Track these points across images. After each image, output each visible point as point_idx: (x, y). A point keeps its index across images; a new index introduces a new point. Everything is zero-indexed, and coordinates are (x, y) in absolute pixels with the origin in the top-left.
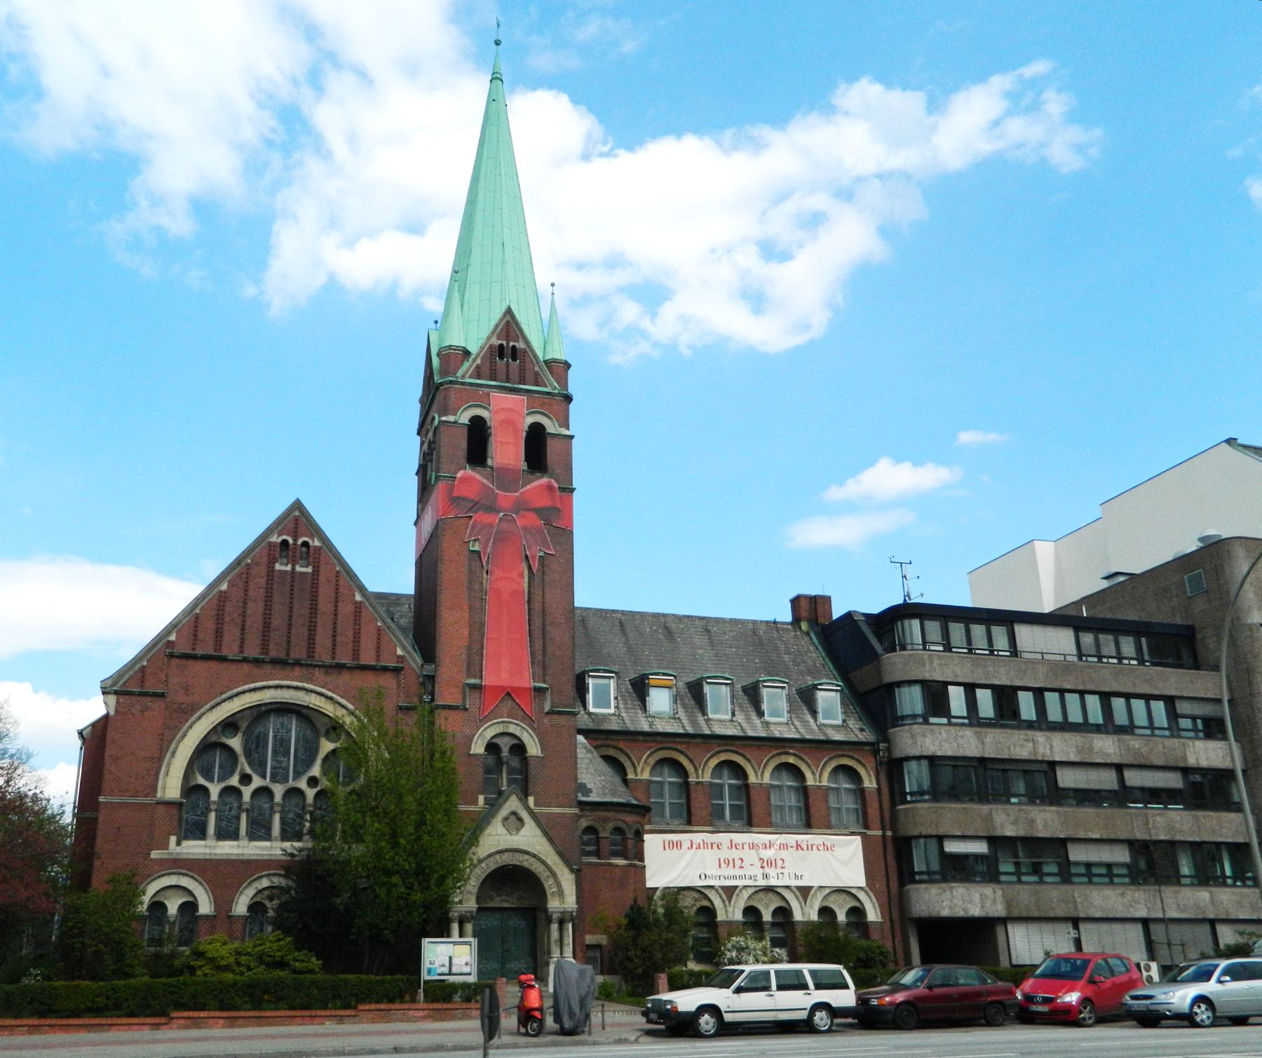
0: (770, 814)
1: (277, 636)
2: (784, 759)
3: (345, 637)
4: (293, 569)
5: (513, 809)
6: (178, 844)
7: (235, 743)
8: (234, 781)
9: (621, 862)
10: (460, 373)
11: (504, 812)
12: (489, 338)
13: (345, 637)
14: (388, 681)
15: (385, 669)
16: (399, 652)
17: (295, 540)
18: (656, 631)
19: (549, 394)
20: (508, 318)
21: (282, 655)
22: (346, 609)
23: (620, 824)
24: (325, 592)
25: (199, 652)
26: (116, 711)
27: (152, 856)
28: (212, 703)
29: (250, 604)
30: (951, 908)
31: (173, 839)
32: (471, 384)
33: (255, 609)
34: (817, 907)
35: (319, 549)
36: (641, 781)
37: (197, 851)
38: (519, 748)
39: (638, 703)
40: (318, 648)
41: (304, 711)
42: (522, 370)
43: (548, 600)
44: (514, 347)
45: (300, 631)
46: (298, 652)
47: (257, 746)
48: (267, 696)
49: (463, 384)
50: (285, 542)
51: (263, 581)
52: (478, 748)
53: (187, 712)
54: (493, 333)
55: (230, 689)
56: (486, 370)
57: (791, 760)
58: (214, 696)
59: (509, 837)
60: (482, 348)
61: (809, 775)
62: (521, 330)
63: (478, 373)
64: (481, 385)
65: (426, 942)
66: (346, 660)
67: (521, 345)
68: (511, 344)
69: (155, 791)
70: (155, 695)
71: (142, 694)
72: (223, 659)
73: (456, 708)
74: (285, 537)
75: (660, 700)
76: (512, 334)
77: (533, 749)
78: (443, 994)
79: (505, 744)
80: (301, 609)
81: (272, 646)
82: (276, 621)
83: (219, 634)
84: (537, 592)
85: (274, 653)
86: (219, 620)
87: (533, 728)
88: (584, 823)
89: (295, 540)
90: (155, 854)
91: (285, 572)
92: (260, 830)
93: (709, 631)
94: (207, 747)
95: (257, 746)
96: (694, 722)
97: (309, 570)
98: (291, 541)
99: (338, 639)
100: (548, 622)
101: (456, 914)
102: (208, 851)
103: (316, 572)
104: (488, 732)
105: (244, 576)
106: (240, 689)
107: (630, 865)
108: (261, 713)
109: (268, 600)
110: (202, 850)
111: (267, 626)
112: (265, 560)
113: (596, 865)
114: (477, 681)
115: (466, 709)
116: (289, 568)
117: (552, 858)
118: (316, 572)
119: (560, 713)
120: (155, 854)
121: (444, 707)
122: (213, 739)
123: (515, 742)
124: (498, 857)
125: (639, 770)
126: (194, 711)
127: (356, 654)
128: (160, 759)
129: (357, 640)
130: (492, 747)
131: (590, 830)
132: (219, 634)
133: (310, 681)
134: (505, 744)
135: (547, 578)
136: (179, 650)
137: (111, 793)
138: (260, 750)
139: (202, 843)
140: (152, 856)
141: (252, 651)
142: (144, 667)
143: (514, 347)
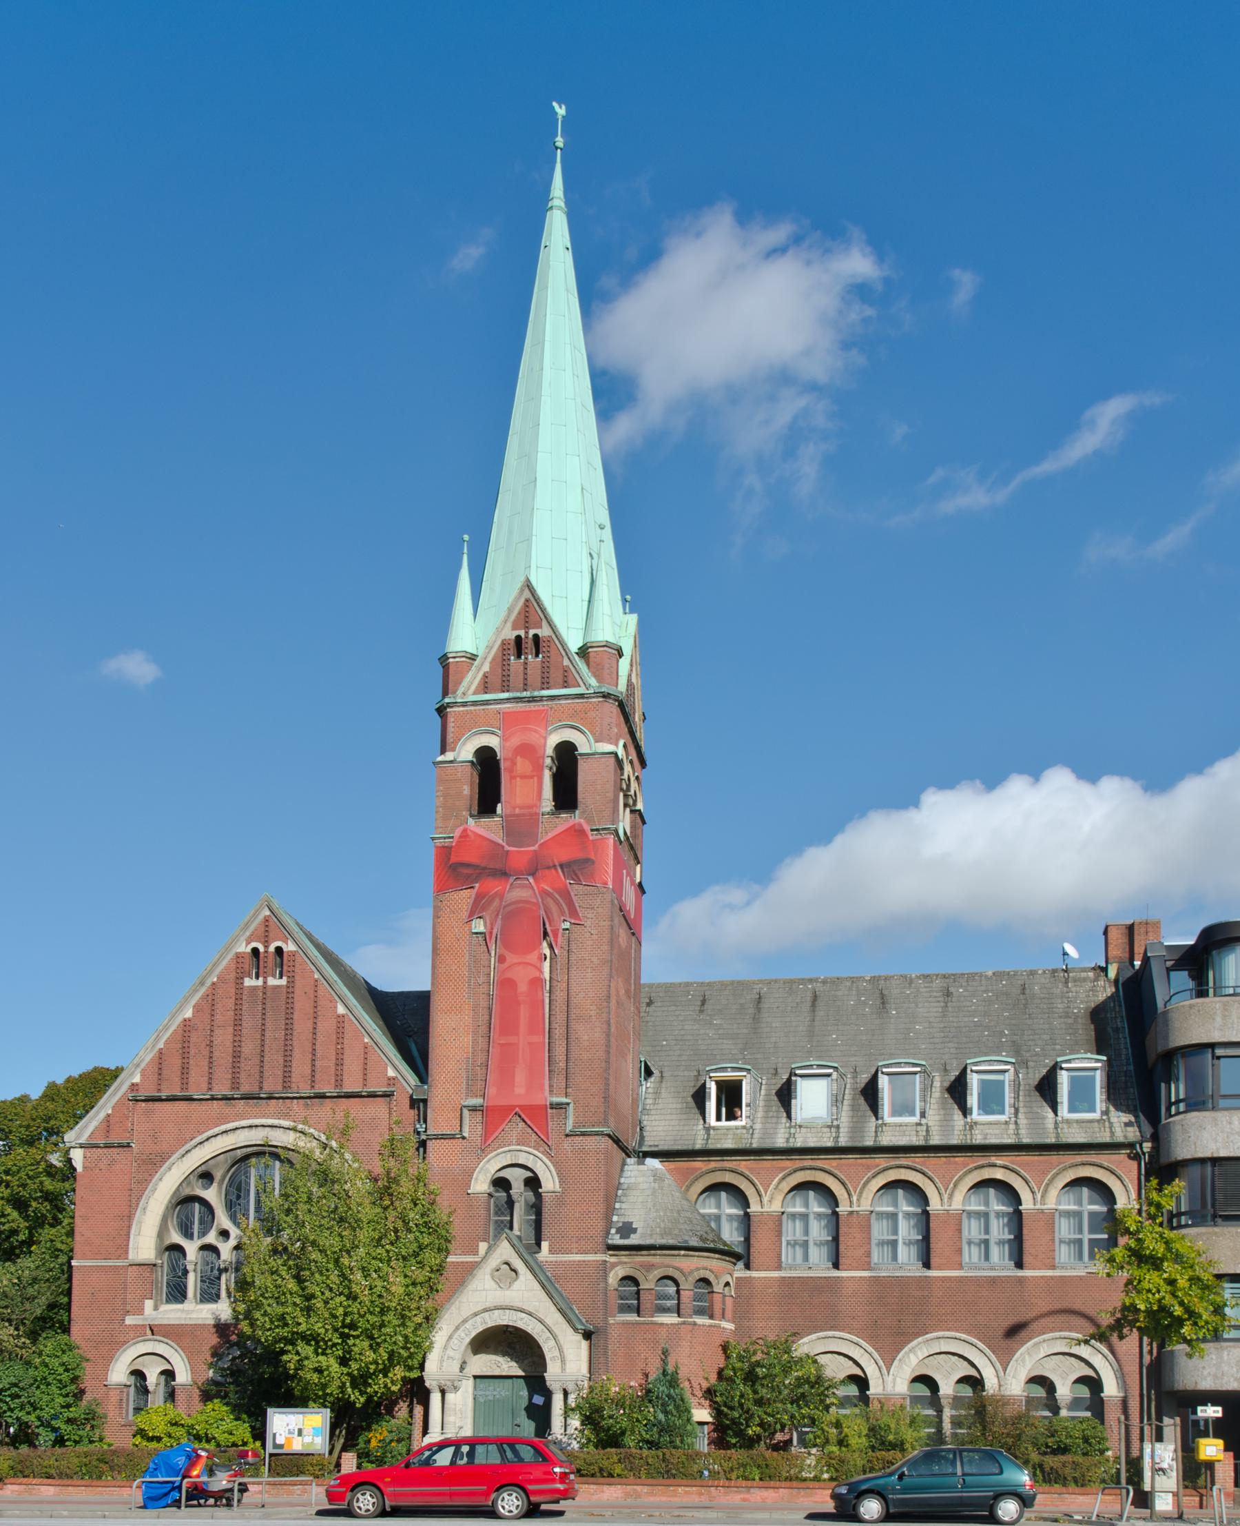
0: (960, 1251)
1: (249, 1067)
2: (987, 1174)
3: (326, 1062)
4: (265, 983)
5: (505, 1258)
6: (156, 1308)
7: (212, 1195)
8: (211, 1238)
9: (670, 1319)
10: (459, 692)
11: (494, 1261)
12: (499, 631)
13: (326, 1062)
14: (378, 1109)
15: (372, 1095)
16: (391, 1073)
17: (266, 947)
18: (864, 1003)
19: (581, 696)
20: (527, 594)
21: (254, 1089)
22: (326, 1027)
23: (703, 1274)
24: (302, 1005)
25: (164, 1095)
26: (84, 1167)
27: (127, 1322)
28: (182, 1151)
29: (217, 1032)
30: (1215, 1377)
31: (149, 1304)
32: (475, 703)
33: (224, 1038)
34: (1024, 1375)
35: (293, 954)
36: (769, 1214)
37: (172, 1315)
38: (533, 1183)
39: (696, 1111)
40: (295, 1076)
41: (279, 1151)
42: (545, 669)
43: (573, 989)
44: (536, 637)
45: (274, 1058)
46: (272, 1084)
47: (239, 1197)
48: (256, 1137)
49: (464, 704)
50: (255, 951)
51: (230, 1003)
52: (481, 1185)
53: (154, 1163)
54: (506, 621)
55: (200, 1133)
56: (496, 680)
57: (999, 1174)
58: (183, 1140)
59: (499, 1293)
60: (490, 648)
61: (1025, 1195)
62: (543, 610)
63: (485, 687)
64: (487, 702)
65: (270, 1411)
66: (329, 1089)
67: (544, 632)
68: (532, 632)
69: (127, 1252)
70: (121, 1146)
71: (107, 1146)
72: (190, 1099)
73: (452, 1137)
74: (254, 945)
75: (813, 1099)
76: (532, 618)
77: (549, 1183)
78: (290, 1465)
79: (517, 1178)
80: (275, 1034)
81: (243, 1077)
82: (249, 1048)
83: (185, 1070)
84: (561, 976)
85: (246, 1088)
86: (185, 1055)
87: (550, 1157)
88: (620, 1272)
89: (266, 947)
90: (129, 1320)
91: (255, 988)
92: (209, 1295)
93: (948, 994)
94: (184, 1201)
95: (239, 1197)
96: (946, 1122)
97: (284, 982)
98: (262, 949)
99: (317, 1063)
100: (573, 1016)
101: (434, 1383)
102: (184, 1316)
103: (291, 982)
104: (490, 1166)
105: (210, 998)
106: (210, 1133)
107: (684, 1323)
108: (243, 1159)
109: (237, 1024)
110: (179, 1315)
111: (236, 1056)
112: (233, 975)
113: (638, 1323)
114: (479, 1101)
115: (464, 1138)
116: (260, 982)
117: (553, 1317)
118: (291, 982)
119: (583, 1134)
120: (129, 1320)
121: (438, 1137)
122: (187, 1191)
123: (529, 1174)
124: (486, 1315)
125: (766, 1199)
126: (164, 1160)
127: (339, 1082)
128: (130, 1217)
129: (339, 1063)
130: (501, 1183)
131: (630, 1279)
132: (185, 1070)
133: (286, 1116)
134: (517, 1178)
135: (573, 958)
136: (143, 1094)
137: (84, 1258)
138: (242, 1201)
139: (179, 1306)
140: (127, 1322)
141: (222, 1089)
142: (109, 1115)
143: (536, 637)
